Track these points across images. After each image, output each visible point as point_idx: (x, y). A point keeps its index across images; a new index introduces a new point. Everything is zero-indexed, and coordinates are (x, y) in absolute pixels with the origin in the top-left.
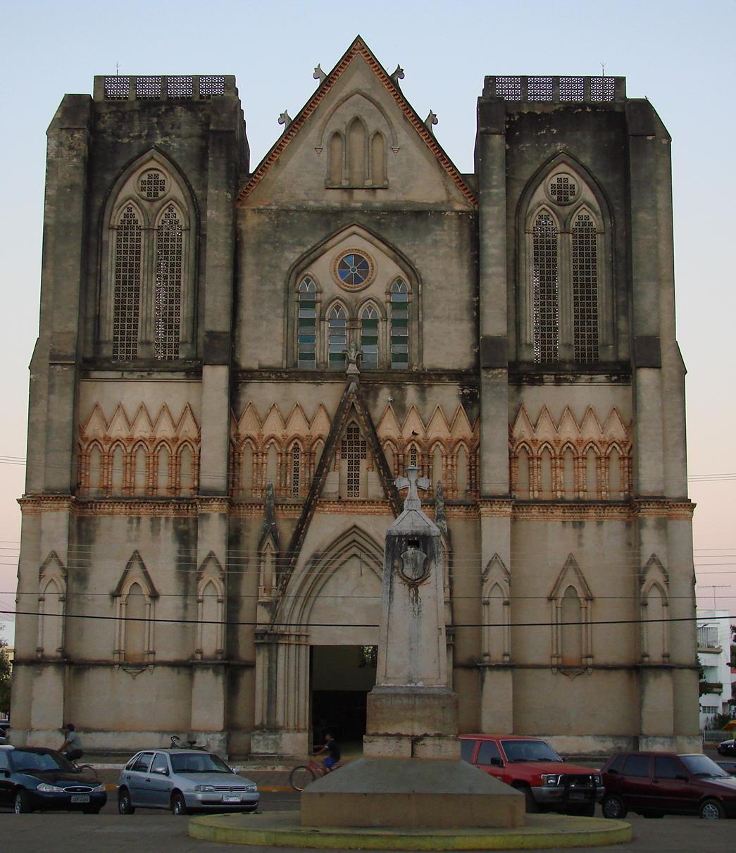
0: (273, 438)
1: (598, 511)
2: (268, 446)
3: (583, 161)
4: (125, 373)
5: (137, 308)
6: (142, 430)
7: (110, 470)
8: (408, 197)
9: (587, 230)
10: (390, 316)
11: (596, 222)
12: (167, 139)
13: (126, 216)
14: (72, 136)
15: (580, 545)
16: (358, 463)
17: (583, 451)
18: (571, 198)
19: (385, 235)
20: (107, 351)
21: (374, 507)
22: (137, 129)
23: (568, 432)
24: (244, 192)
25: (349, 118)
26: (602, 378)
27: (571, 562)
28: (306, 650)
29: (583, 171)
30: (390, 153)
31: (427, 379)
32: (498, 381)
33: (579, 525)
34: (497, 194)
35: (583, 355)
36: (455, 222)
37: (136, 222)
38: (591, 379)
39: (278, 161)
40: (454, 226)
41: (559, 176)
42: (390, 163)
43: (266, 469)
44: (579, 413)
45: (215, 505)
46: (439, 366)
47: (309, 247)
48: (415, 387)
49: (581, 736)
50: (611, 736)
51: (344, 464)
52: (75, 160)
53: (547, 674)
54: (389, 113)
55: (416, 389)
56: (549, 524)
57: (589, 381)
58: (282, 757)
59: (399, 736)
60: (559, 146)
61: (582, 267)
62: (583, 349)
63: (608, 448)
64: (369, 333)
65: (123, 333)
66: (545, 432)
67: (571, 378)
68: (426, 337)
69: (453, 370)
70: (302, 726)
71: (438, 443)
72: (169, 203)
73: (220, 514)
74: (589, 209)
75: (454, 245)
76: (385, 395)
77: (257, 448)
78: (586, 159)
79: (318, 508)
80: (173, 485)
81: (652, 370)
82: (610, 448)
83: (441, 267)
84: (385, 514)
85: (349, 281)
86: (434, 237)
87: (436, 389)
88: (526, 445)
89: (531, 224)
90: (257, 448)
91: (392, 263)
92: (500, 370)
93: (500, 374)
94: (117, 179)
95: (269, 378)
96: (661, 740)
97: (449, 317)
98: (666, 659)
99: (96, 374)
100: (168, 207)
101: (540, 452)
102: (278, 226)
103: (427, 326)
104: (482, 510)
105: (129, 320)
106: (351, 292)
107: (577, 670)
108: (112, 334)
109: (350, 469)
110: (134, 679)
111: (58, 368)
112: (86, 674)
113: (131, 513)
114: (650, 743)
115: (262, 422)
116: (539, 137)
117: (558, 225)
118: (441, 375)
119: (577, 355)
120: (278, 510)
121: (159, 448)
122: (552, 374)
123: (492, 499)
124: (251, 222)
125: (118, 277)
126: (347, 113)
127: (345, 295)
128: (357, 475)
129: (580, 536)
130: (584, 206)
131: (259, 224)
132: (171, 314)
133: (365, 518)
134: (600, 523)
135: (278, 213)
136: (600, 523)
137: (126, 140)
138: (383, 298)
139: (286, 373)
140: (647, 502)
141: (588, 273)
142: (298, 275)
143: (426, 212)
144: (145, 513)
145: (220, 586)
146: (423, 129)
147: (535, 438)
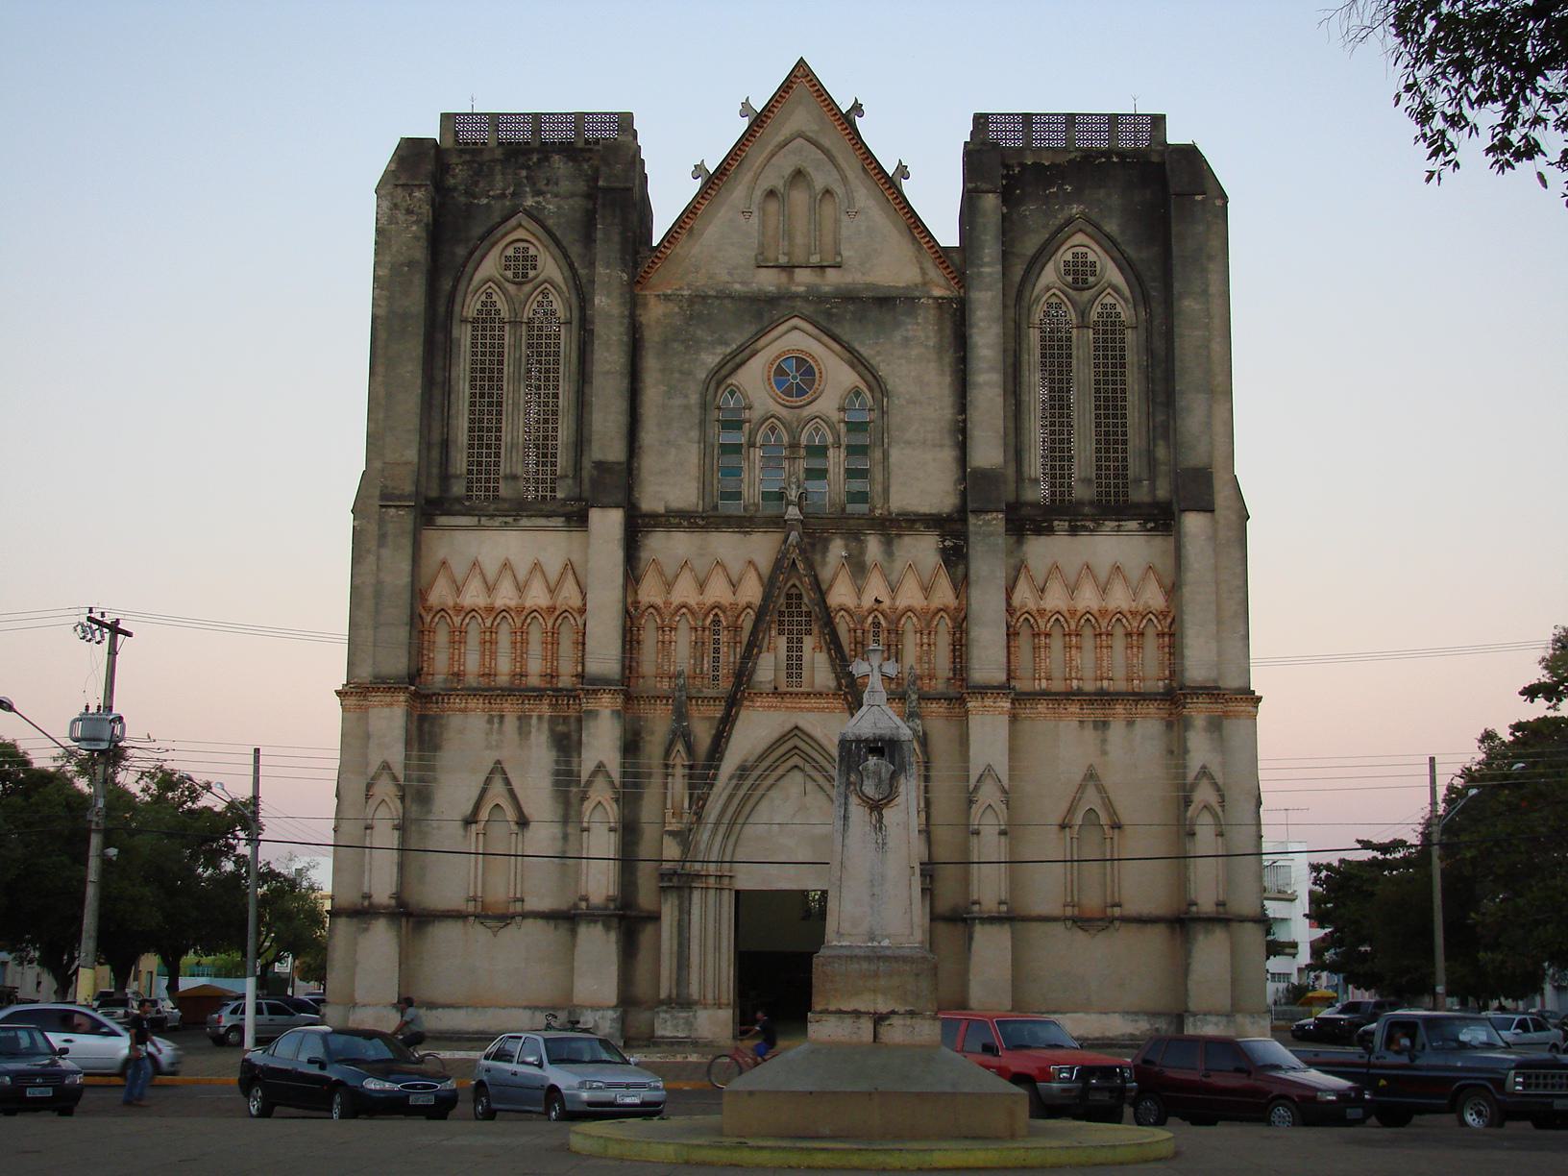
1: (1128, 706)
2: (678, 618)
4: (483, 519)
5: (499, 430)
8: (869, 279)
9: (1113, 324)
10: (844, 441)
11: (1125, 313)
12: (541, 199)
13: (484, 304)
14: (410, 195)
15: (1104, 753)
18: (1091, 279)
19: (838, 331)
20: (458, 489)
23: (1088, 599)
24: (645, 272)
25: (788, 171)
26: (1133, 525)
29: (1107, 244)
33: (1102, 725)
34: (990, 274)
35: (1108, 494)
36: (932, 312)
38: (1119, 526)
41: (1076, 250)
42: (844, 232)
45: (606, 699)
46: (910, 508)
47: (734, 346)
48: (879, 537)
49: (1105, 1013)
56: (1062, 724)
59: (857, 1014)
61: (1105, 374)
62: (1108, 485)
64: (816, 464)
66: (1055, 599)
67: (1091, 525)
70: (724, 1000)
71: (909, 613)
73: (613, 711)
76: (837, 549)
78: (1112, 227)
79: (746, 703)
80: (549, 671)
82: (1145, 621)
85: (788, 393)
86: (905, 333)
91: (846, 368)
92: (995, 514)
93: (994, 519)
94: (471, 253)
95: (678, 526)
96: (1214, 1019)
98: (1221, 909)
99: (443, 520)
101: (1049, 626)
102: (691, 317)
103: (895, 454)
105: (489, 447)
106: (791, 408)
107: (1100, 923)
109: (789, 649)
110: (495, 936)
111: (392, 511)
113: (491, 710)
114: (1199, 1023)
115: (669, 586)
116: (1047, 196)
117: (1073, 316)
118: (914, 521)
119: (1099, 494)
121: (529, 621)
122: (1065, 521)
123: (983, 690)
125: (473, 387)
126: (786, 163)
127: (783, 412)
128: (800, 658)
129: (1104, 741)
130: (1109, 290)
132: (546, 438)
134: (1130, 723)
135: (691, 301)
136: (1130, 723)
137: (485, 201)
138: (835, 416)
139: (703, 518)
143: (894, 299)
144: (510, 709)
146: (889, 186)
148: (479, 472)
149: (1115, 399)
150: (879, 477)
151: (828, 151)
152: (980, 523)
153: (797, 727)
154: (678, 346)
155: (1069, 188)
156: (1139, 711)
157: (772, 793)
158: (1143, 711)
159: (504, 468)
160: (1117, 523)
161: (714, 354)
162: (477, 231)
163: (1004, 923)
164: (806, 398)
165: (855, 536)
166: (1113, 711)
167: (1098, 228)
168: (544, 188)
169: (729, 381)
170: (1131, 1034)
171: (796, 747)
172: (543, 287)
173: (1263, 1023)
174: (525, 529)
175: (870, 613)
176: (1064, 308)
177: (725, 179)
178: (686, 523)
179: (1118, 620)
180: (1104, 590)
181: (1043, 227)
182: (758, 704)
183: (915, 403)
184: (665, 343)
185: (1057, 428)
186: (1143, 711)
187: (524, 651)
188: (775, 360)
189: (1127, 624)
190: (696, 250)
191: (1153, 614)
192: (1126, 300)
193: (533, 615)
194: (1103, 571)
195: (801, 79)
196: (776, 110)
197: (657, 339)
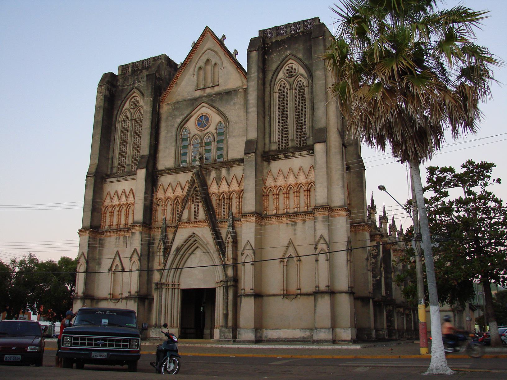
1: (303, 217)
3: (299, 56)
4: (118, 178)
8: (227, 88)
9: (301, 87)
10: (216, 139)
11: (305, 82)
12: (140, 83)
15: (295, 234)
16: (198, 205)
17: (297, 188)
18: (294, 74)
19: (214, 105)
20: (115, 170)
22: (130, 82)
23: (291, 180)
24: (163, 98)
25: (205, 60)
26: (305, 152)
27: (291, 243)
29: (298, 60)
30: (220, 70)
31: (230, 164)
32: (251, 159)
33: (294, 225)
34: (254, 76)
35: (300, 144)
36: (242, 93)
37: (128, 118)
38: (301, 153)
39: (177, 83)
40: (242, 95)
41: (289, 65)
42: (220, 75)
44: (296, 171)
45: (137, 228)
46: (234, 158)
47: (185, 115)
48: (226, 168)
49: (294, 329)
50: (308, 329)
51: (193, 206)
52: (101, 97)
53: (280, 298)
54: (220, 55)
55: (226, 170)
57: (300, 155)
58: (161, 339)
60: (288, 52)
61: (299, 103)
62: (300, 141)
63: (308, 186)
64: (208, 147)
65: (121, 162)
66: (281, 182)
67: (291, 154)
68: (230, 146)
69: (241, 158)
73: (139, 232)
74: (302, 77)
75: (242, 103)
76: (213, 174)
78: (300, 56)
79: (179, 226)
81: (321, 143)
82: (310, 186)
83: (236, 114)
86: (234, 102)
87: (234, 168)
89: (276, 88)
91: (218, 116)
92: (252, 154)
93: (252, 155)
94: (122, 103)
95: (168, 173)
96: (323, 330)
97: (239, 135)
98: (317, 289)
99: (108, 180)
100: (139, 110)
101: (278, 191)
102: (174, 109)
103: (230, 140)
106: (202, 131)
107: (292, 296)
108: (117, 164)
109: (195, 208)
111: (89, 178)
112: (99, 303)
113: (117, 235)
114: (318, 332)
115: (165, 191)
116: (279, 50)
117: (288, 87)
118: (235, 161)
119: (297, 144)
121: (129, 207)
122: (282, 154)
123: (246, 215)
124: (165, 109)
125: (121, 140)
126: (204, 58)
127: (199, 133)
129: (295, 230)
130: (300, 76)
131: (168, 110)
132: (138, 152)
133: (197, 229)
134: (304, 223)
135: (175, 104)
136: (304, 223)
137: (126, 87)
138: (214, 131)
139: (174, 169)
140: (317, 208)
141: (302, 106)
142: (181, 128)
143: (231, 91)
144: (121, 234)
145: (137, 263)
146: (232, 57)
149: (302, 111)
150: (225, 149)
151: (216, 52)
152: (247, 157)
153: (194, 233)
154: (170, 118)
155: (286, 46)
156: (306, 218)
157: (192, 256)
158: (308, 218)
159: (127, 163)
160: (300, 153)
161: (180, 119)
162: (124, 96)
163: (252, 297)
164: (206, 127)
165: (218, 169)
166: (298, 219)
167: (295, 56)
168: (141, 80)
169: (185, 126)
170: (304, 337)
173: (348, 332)
174: (129, 180)
176: (285, 85)
177: (186, 66)
178: (170, 172)
179: (301, 186)
180: (296, 177)
181: (278, 60)
182: (183, 226)
183: (236, 123)
184: (167, 118)
185: (283, 124)
186: (308, 218)
188: (197, 117)
190: (179, 89)
192: (305, 78)
194: (296, 171)
195: (207, 32)
196: (200, 43)
197: (165, 117)
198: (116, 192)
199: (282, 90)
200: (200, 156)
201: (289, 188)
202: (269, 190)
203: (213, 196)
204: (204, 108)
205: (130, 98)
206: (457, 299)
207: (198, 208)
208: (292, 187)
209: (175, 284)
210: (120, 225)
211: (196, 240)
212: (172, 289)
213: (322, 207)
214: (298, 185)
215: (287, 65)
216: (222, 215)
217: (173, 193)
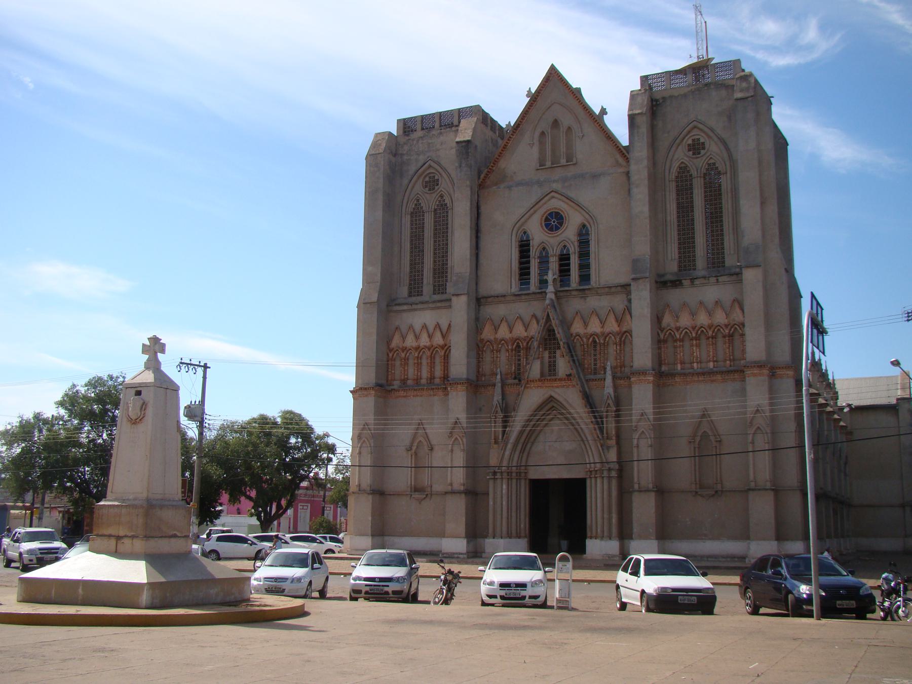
0: (503, 340)
2: (500, 346)
6: (424, 341)
7: (406, 368)
13: (416, 205)
16: (555, 353)
21: (563, 382)
23: (703, 319)
28: (525, 483)
41: (691, 138)
43: (499, 362)
56: (688, 387)
59: (110, 536)
66: (685, 321)
70: (523, 534)
71: (610, 335)
72: (440, 193)
77: (493, 347)
82: (732, 329)
84: (570, 387)
88: (671, 332)
90: (493, 347)
101: (682, 336)
104: (632, 379)
109: (550, 357)
115: (496, 329)
120: (508, 388)
125: (411, 244)
133: (557, 390)
146: (597, 120)
147: (678, 326)
148: (415, 284)
171: (553, 407)
172: (440, 193)
175: (591, 336)
179: (719, 330)
180: (710, 314)
182: (532, 386)
187: (432, 367)
189: (723, 332)
191: (737, 325)
193: (436, 350)
198: (411, 327)
199: (682, 177)
200: (554, 277)
201: (699, 332)
202: (683, 332)
203: (578, 339)
204: (553, 200)
205: (423, 176)
206: (254, 486)
207: (555, 357)
208: (687, 331)
209: (520, 473)
210: (421, 378)
211: (553, 407)
212: (517, 479)
213: (760, 365)
214: (714, 327)
215: (689, 138)
216: (593, 369)
217: (511, 332)
